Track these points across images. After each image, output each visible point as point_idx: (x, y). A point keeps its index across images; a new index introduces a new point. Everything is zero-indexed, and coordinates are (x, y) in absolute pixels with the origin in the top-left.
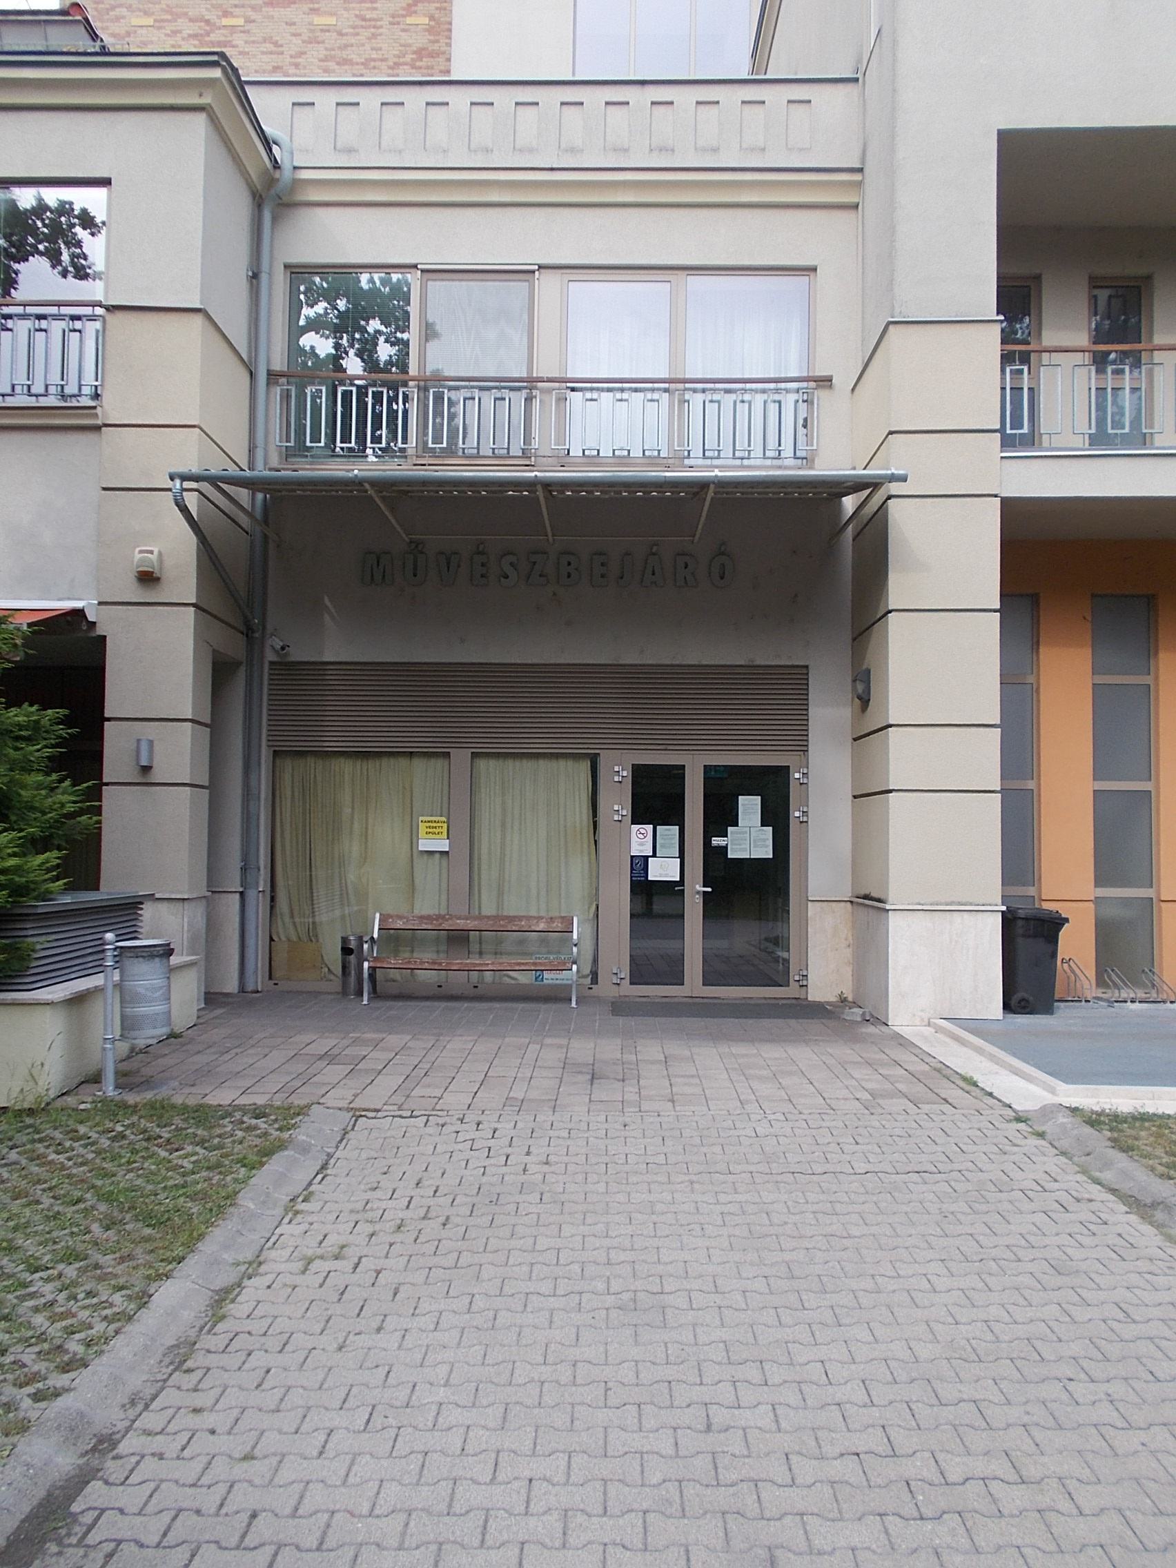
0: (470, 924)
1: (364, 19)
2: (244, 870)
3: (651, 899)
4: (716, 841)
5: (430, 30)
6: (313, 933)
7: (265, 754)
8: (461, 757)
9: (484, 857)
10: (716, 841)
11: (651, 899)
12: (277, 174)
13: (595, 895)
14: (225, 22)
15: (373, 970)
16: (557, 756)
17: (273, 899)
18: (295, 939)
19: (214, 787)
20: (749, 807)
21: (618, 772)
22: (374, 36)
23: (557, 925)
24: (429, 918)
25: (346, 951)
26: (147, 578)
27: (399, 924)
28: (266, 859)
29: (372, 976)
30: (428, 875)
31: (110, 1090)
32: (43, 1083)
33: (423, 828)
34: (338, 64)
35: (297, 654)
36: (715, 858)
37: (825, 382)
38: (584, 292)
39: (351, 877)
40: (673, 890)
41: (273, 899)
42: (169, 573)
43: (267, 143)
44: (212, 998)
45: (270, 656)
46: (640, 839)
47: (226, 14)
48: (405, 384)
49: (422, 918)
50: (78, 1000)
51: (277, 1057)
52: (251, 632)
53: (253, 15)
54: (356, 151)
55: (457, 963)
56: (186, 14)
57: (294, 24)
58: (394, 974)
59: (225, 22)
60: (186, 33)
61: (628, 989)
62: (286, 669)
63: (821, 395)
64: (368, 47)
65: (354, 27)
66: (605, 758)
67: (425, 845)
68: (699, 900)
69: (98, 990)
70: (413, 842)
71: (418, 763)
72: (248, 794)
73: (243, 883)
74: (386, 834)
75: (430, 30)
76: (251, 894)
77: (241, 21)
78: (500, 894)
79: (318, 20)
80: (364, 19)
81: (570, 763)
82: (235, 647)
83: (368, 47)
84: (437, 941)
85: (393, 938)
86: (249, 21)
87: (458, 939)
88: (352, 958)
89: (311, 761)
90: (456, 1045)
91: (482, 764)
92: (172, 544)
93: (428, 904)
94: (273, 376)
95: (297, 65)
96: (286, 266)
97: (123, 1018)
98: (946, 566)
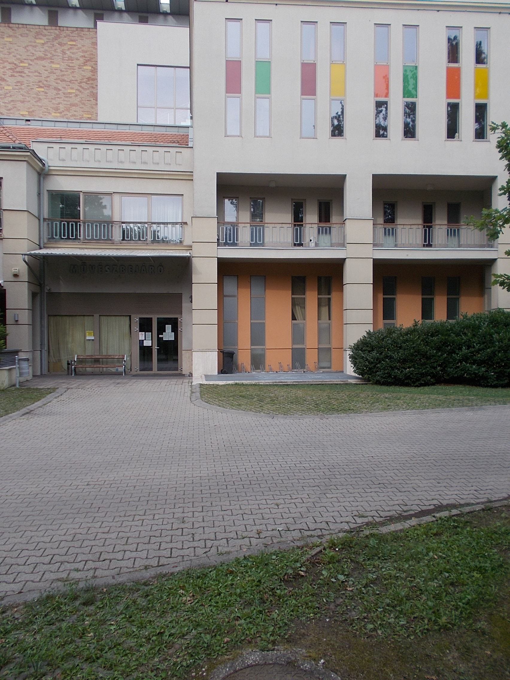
0: (99, 357)
1: (69, 66)
2: (41, 345)
3: (145, 352)
4: (160, 336)
5: (92, 71)
6: (60, 361)
7: (46, 316)
8: (97, 316)
9: (103, 340)
10: (160, 336)
11: (145, 352)
12: (44, 168)
13: (130, 350)
14: (21, 65)
15: (75, 368)
16: (121, 316)
17: (49, 352)
18: (55, 361)
19: (33, 325)
20: (168, 327)
21: (136, 320)
22: (73, 72)
23: (121, 357)
24: (89, 356)
25: (68, 364)
26: (16, 276)
27: (82, 357)
28: (48, 342)
29: (75, 370)
30: (89, 346)
31: (18, 386)
32: (5, 385)
33: (87, 334)
34: (61, 81)
35: (53, 290)
36: (160, 340)
37: (186, 223)
38: (125, 199)
39: (69, 346)
40: (150, 348)
41: (49, 352)
42: (21, 275)
43: (40, 160)
44: (34, 376)
45: (46, 291)
46: (141, 336)
47: (22, 62)
48: (79, 222)
49: (87, 356)
50: (10, 370)
51: (51, 383)
52: (41, 285)
53: (31, 63)
54: (65, 160)
55: (95, 366)
56: (8, 61)
57: (45, 66)
58: (81, 369)
59: (21, 65)
60: (8, 67)
61: (139, 372)
62: (51, 294)
63: (185, 226)
64: (71, 76)
65: (66, 69)
66: (132, 316)
67: (88, 338)
68: (156, 350)
69: (15, 368)
70: (85, 337)
71: (86, 318)
72: (42, 326)
73: (41, 348)
74: (78, 336)
75: (92, 71)
76: (43, 351)
77: (27, 65)
78: (107, 350)
79: (54, 66)
80: (69, 66)
81: (124, 317)
82: (37, 289)
83: (71, 76)
84: (91, 362)
85: (81, 361)
86: (30, 65)
87: (97, 361)
88: (70, 366)
89: (58, 317)
90: (91, 381)
91: (102, 318)
92: (22, 268)
93: (89, 352)
94: (44, 219)
95: (47, 81)
96: (47, 190)
97: (20, 373)
98: (205, 273)
